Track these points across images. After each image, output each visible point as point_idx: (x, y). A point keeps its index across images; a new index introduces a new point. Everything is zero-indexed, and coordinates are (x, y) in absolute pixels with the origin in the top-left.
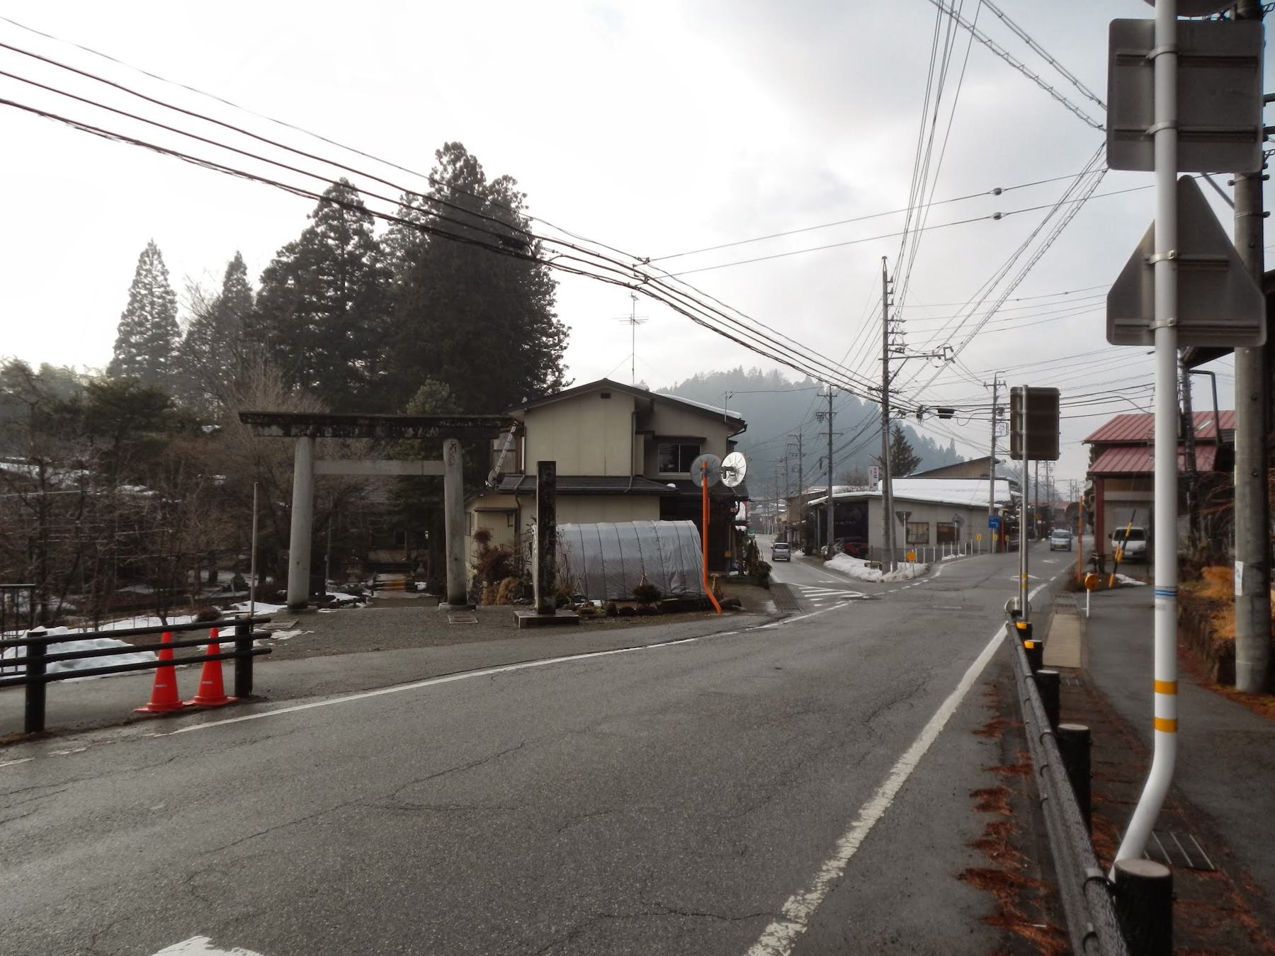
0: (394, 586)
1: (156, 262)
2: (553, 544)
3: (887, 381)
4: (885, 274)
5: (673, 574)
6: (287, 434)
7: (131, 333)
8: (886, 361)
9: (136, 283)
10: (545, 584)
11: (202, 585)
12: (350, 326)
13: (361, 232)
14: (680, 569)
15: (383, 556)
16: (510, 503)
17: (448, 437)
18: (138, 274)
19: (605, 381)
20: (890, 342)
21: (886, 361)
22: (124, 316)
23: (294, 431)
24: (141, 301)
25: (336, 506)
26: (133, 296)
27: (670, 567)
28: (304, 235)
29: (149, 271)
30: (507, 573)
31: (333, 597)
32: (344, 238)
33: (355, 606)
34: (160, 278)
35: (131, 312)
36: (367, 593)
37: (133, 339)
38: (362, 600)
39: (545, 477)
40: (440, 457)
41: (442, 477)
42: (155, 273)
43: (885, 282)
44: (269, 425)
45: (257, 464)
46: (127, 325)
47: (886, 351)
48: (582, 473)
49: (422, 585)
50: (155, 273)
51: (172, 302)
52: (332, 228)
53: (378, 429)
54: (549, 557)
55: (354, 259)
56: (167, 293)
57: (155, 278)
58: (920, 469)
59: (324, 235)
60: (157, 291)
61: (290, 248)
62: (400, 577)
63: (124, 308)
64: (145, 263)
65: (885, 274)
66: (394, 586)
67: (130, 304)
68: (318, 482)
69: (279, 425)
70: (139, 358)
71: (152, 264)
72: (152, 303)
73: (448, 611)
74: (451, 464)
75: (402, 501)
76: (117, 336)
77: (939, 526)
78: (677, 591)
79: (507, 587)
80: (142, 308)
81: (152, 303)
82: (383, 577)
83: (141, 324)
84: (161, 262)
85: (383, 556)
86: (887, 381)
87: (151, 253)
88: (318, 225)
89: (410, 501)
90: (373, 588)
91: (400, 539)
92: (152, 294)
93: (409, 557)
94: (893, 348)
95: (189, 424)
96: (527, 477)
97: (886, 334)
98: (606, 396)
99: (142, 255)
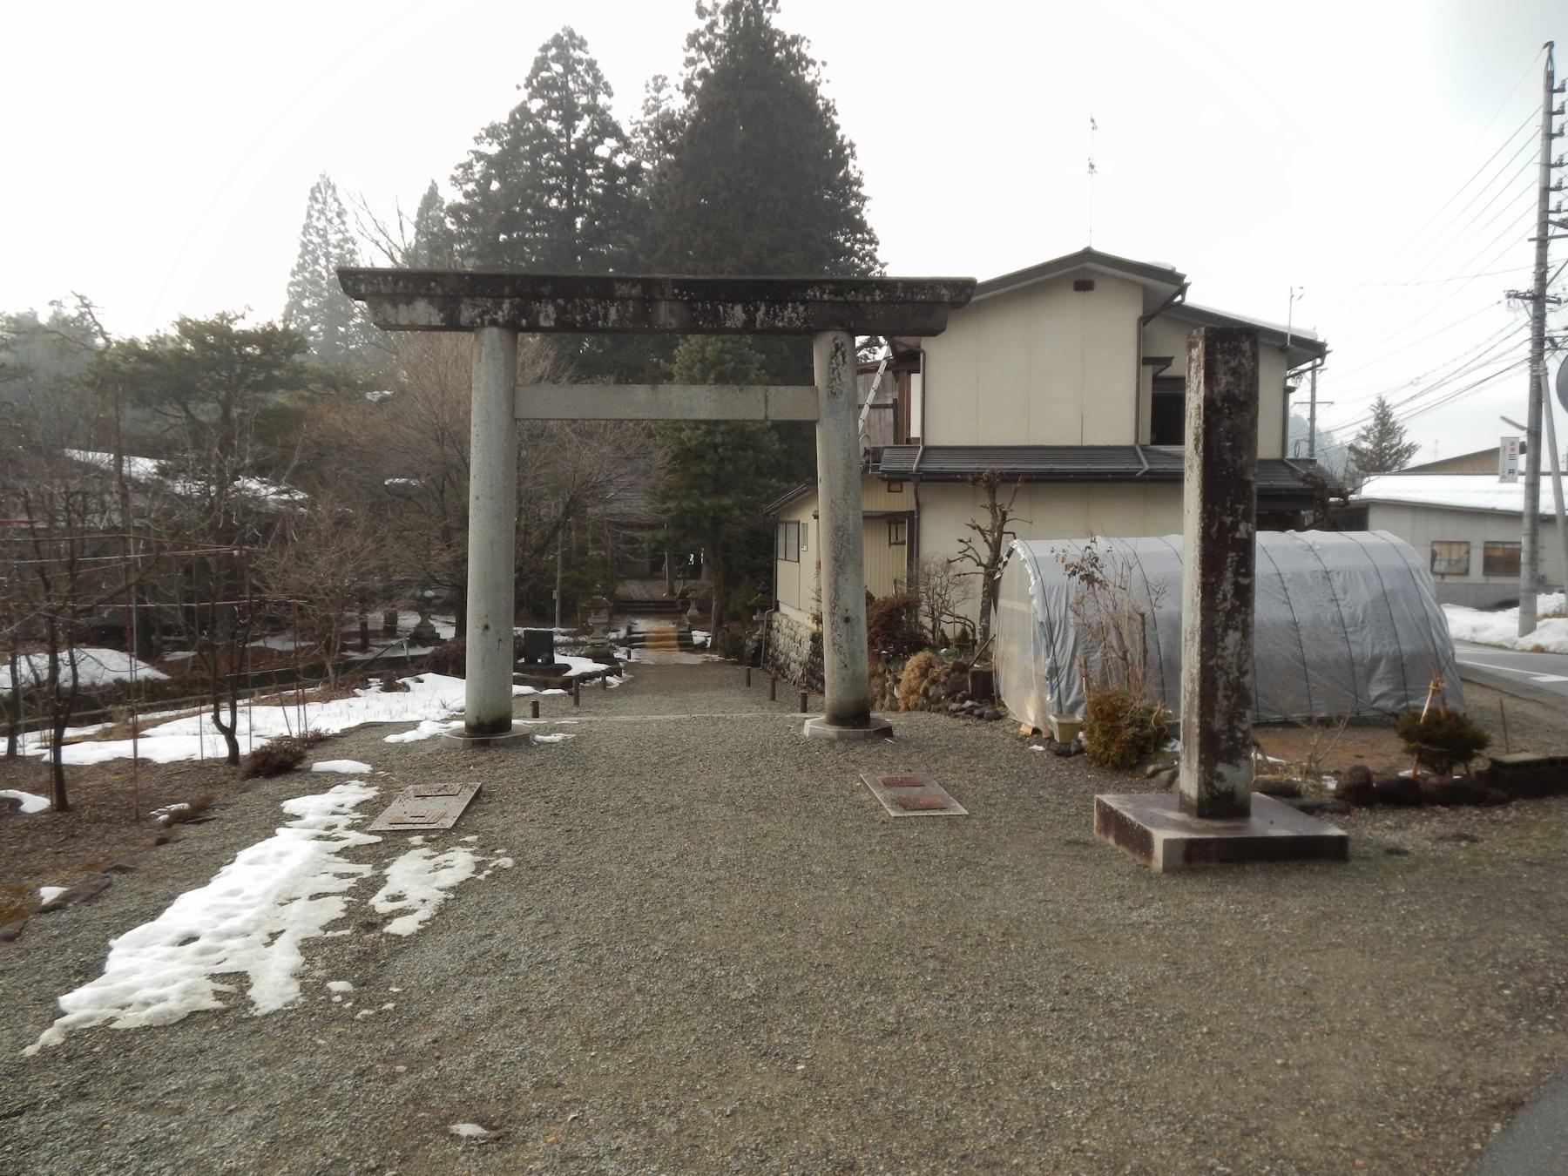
0: (660, 641)
1: (330, 200)
2: (1244, 594)
3: (1541, 279)
4: (1550, 76)
5: (1375, 661)
6: (452, 325)
7: (302, 296)
8: (1543, 242)
9: (307, 227)
10: (1218, 724)
11: (366, 635)
12: (581, 250)
13: (591, 109)
14: (1391, 649)
15: (633, 590)
16: (902, 501)
17: (824, 328)
18: (309, 216)
19: (1088, 255)
20: (1552, 206)
21: (1543, 242)
22: (294, 274)
23: (466, 314)
24: (314, 251)
25: (567, 513)
26: (304, 245)
27: (1366, 644)
28: (512, 116)
29: (322, 212)
30: (918, 643)
31: (568, 668)
32: (569, 120)
33: (605, 684)
34: (336, 221)
35: (302, 268)
36: (620, 654)
37: (306, 303)
38: (615, 671)
39: (1224, 381)
40: (804, 376)
41: (812, 425)
42: (329, 215)
43: (1550, 91)
44: (409, 300)
45: (440, 441)
46: (298, 284)
47: (1544, 223)
48: (1032, 443)
49: (698, 636)
50: (329, 215)
51: (352, 252)
52: (553, 104)
53: (663, 308)
54: (1232, 638)
55: (584, 152)
56: (346, 240)
57: (330, 221)
58: (1415, 460)
59: (543, 114)
60: (334, 238)
61: (493, 132)
62: (667, 626)
63: (293, 261)
64: (316, 200)
65: (1550, 76)
66: (660, 641)
67: (302, 256)
68: (527, 440)
69: (430, 297)
70: (314, 328)
71: (325, 203)
72: (327, 255)
73: (831, 742)
74: (833, 394)
75: (671, 504)
76: (286, 299)
77: (1489, 546)
78: (1388, 704)
79: (924, 673)
80: (316, 261)
81: (327, 255)
82: (643, 625)
83: (315, 283)
84: (336, 200)
85: (633, 590)
86: (1541, 279)
87: (321, 192)
88: (531, 97)
89: (685, 504)
90: (630, 642)
91: (656, 566)
92: (327, 243)
93: (672, 592)
94: (1554, 217)
95: (339, 385)
96: (926, 449)
97: (1546, 191)
98: (1084, 286)
99: (313, 191)
